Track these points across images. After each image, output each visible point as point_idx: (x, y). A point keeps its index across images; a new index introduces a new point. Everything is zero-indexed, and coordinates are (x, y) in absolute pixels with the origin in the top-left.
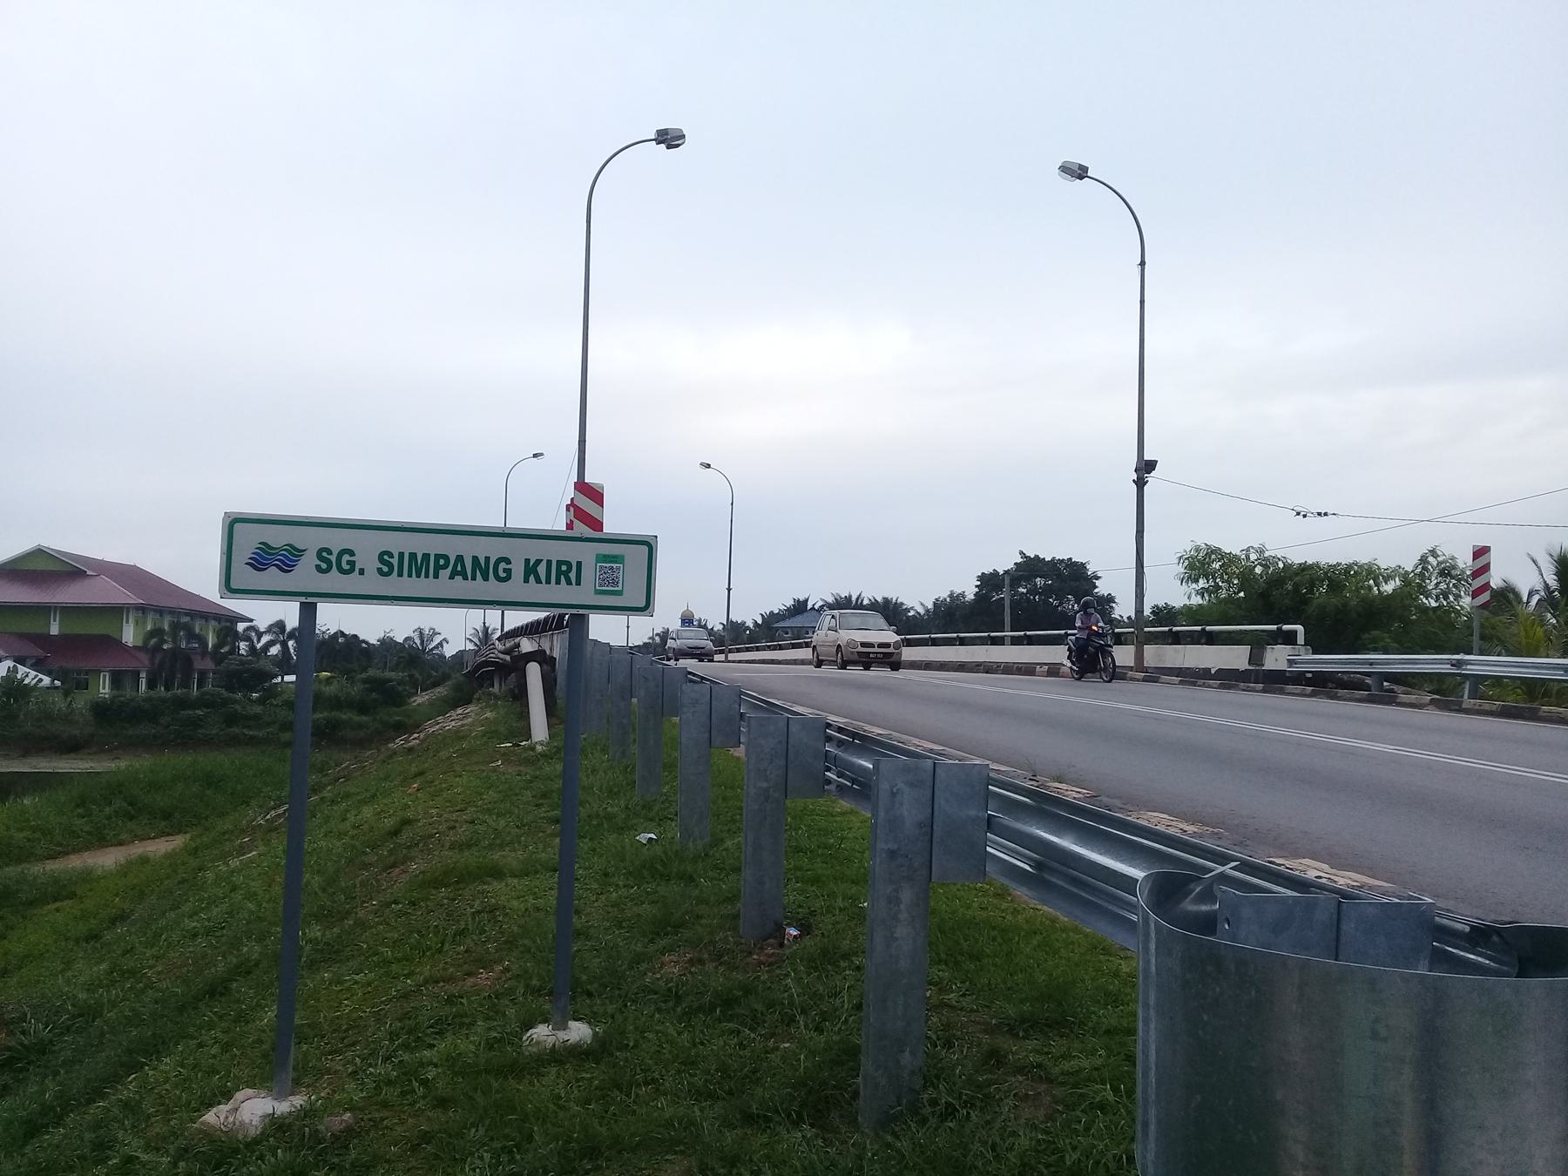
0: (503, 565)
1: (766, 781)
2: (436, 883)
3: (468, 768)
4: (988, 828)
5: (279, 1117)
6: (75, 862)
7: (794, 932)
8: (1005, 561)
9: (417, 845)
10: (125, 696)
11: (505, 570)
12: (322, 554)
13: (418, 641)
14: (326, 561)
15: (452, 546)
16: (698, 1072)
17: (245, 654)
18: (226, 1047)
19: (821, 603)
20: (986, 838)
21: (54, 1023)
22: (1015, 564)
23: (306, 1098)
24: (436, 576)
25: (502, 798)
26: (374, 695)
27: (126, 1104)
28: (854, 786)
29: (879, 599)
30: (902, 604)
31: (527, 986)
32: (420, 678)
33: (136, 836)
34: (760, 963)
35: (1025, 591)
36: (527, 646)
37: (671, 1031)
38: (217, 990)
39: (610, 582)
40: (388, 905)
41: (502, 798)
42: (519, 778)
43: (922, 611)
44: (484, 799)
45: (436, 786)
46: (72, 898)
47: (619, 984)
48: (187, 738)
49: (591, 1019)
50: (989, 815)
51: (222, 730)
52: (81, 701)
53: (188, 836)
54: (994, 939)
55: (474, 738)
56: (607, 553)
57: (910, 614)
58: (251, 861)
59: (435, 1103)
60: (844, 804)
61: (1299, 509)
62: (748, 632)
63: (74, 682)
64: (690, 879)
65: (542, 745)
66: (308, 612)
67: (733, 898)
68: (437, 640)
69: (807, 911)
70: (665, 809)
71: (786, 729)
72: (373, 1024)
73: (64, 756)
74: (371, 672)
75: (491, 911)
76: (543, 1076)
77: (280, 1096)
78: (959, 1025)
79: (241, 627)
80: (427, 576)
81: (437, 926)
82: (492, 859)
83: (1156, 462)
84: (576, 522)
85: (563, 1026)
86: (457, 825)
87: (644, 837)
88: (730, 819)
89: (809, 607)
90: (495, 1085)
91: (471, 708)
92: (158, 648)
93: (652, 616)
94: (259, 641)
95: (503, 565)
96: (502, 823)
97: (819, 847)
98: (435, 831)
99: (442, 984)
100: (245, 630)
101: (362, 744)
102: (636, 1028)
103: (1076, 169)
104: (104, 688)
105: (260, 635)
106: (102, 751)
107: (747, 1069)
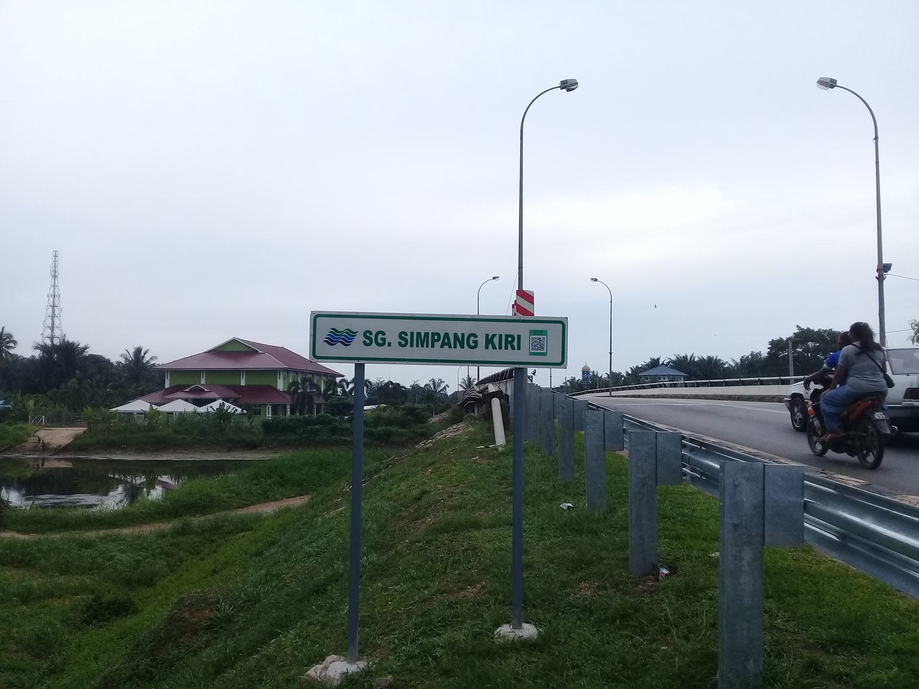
0: (472, 339)
1: (643, 473)
2: (442, 531)
3: (459, 460)
4: (805, 509)
5: (350, 675)
6: (253, 510)
7: (665, 571)
8: (787, 332)
9: (431, 506)
10: (279, 418)
11: (474, 342)
12: (367, 334)
13: (432, 387)
14: (370, 338)
15: (441, 328)
16: (607, 662)
17: (340, 394)
18: (324, 626)
19: (668, 361)
20: (803, 518)
21: (234, 605)
22: (794, 333)
23: (366, 664)
24: (433, 346)
25: (479, 479)
26: (409, 417)
27: (268, 658)
28: (703, 478)
29: (705, 358)
30: (720, 360)
31: (496, 599)
32: (434, 407)
33: (284, 496)
34: (644, 591)
35: (801, 350)
36: (492, 388)
37: (588, 634)
38: (320, 590)
39: (538, 348)
40: (414, 543)
41: (479, 479)
42: (489, 467)
43: (733, 364)
44: (468, 480)
45: (441, 471)
46: (251, 531)
47: (553, 600)
48: (311, 441)
49: (536, 623)
50: (805, 500)
51: (329, 437)
52: (257, 421)
53: (310, 496)
54: (806, 582)
55: (462, 442)
56: (537, 329)
57: (725, 366)
58: (341, 512)
59: (442, 672)
60: (692, 488)
62: (623, 379)
63: (253, 411)
64: (595, 534)
65: (502, 447)
66: (360, 369)
67: (624, 547)
68: (443, 386)
69: (673, 557)
70: (577, 488)
71: (655, 440)
72: (405, 618)
73: (248, 451)
74: (407, 404)
75: (474, 549)
76: (508, 658)
77: (352, 661)
78: (786, 642)
79: (338, 379)
80: (427, 346)
81: (442, 557)
82: (474, 517)
83: (892, 264)
84: (518, 313)
85: (518, 626)
86: (453, 495)
87: (565, 506)
88: (618, 495)
89: (661, 363)
90: (478, 664)
91: (461, 425)
92: (295, 392)
93: (566, 368)
94: (347, 387)
95: (472, 339)
96: (479, 495)
97: (678, 515)
98: (441, 498)
99: (445, 594)
100: (340, 382)
101: (403, 445)
102: (566, 631)
103: (829, 82)
104: (269, 414)
105: (348, 384)
106: (268, 448)
107: (639, 663)
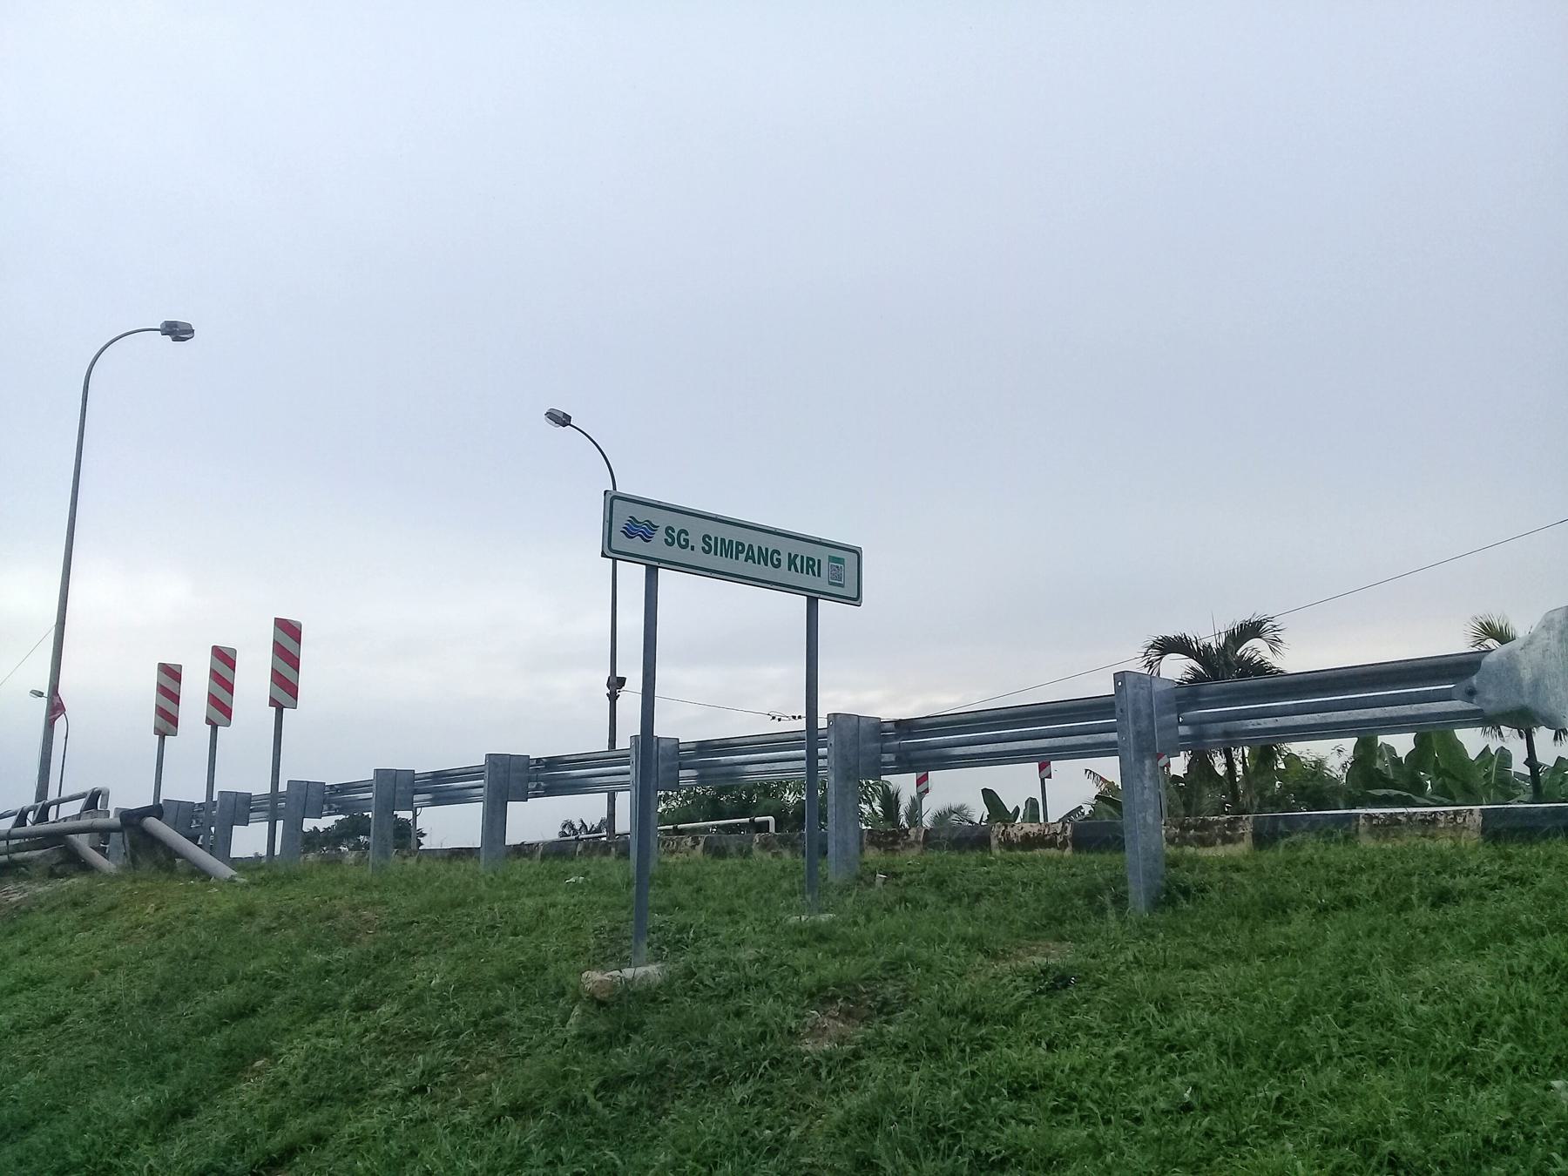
24: (737, 558)
61: (774, 714)
